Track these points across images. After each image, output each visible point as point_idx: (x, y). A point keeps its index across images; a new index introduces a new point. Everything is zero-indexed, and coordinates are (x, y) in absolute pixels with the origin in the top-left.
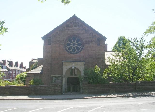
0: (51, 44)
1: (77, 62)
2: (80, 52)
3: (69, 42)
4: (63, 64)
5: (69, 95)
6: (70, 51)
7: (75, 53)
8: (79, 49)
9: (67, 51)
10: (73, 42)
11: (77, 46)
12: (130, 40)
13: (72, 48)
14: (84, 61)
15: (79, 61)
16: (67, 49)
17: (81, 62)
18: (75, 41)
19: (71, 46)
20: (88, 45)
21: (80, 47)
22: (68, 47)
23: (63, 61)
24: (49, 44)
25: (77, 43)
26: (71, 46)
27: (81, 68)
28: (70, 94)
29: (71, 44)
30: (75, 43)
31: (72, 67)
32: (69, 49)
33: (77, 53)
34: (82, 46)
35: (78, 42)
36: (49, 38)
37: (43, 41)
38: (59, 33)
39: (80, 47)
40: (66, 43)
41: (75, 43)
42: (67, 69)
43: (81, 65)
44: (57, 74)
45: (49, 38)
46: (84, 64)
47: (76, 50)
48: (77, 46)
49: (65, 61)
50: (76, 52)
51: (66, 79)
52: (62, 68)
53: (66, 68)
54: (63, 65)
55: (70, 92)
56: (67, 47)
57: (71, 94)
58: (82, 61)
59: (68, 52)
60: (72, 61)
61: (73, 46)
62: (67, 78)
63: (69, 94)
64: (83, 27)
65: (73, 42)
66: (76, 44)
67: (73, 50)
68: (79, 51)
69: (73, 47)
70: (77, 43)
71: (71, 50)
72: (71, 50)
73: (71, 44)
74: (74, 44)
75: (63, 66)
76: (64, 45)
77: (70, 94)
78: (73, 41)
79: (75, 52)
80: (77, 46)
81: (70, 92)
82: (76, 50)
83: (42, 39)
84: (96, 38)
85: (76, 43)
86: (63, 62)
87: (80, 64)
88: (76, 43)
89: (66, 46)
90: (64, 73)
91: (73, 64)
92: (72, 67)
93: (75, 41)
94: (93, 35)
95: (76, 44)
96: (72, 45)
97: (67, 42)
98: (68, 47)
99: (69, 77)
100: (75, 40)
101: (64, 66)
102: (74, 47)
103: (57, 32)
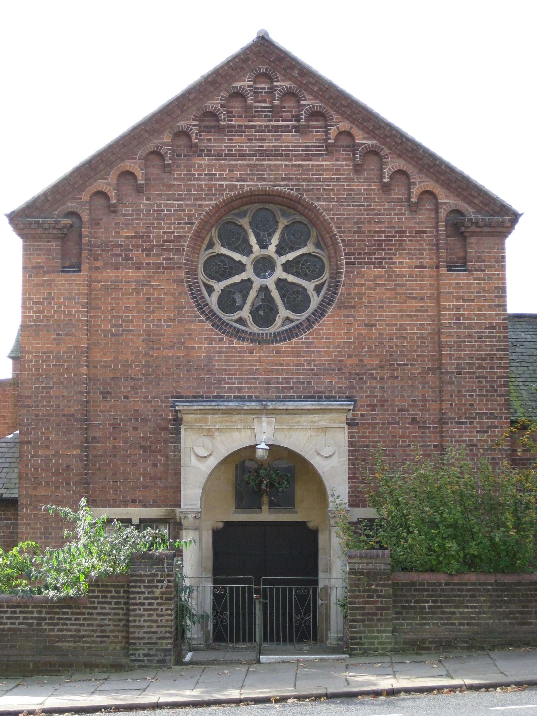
0: (85, 267)
1: (291, 406)
2: (309, 327)
3: (224, 251)
4: (178, 422)
5: (243, 669)
6: (236, 316)
7: (279, 337)
8: (307, 300)
9: (211, 316)
10: (256, 247)
11: (291, 278)
12: (343, 417)
13: (252, 294)
14: (349, 398)
15: (310, 398)
16: (213, 301)
17: (324, 405)
18: (275, 240)
19: (237, 279)
20: (370, 272)
21: (309, 286)
22: (219, 286)
23: (179, 398)
24: (65, 270)
25: (291, 256)
26: (237, 279)
27: (327, 452)
28: (252, 655)
29: (240, 267)
30: (275, 256)
31: (253, 448)
32: (228, 302)
33: (290, 334)
34: (326, 276)
35: (292, 249)
36: (69, 222)
37: (17, 243)
38: (141, 180)
39: (309, 286)
40: (204, 255)
41: (275, 256)
42: (213, 462)
43: (323, 423)
44: (135, 502)
45: (69, 222)
46: (351, 423)
47: (283, 312)
48: (284, 275)
49: (197, 398)
50: (279, 321)
51: (208, 538)
52: (178, 451)
53: (202, 452)
54: (178, 433)
55: (251, 639)
56: (210, 289)
57: (258, 662)
58: (330, 398)
59: (220, 325)
60: (250, 399)
61: (257, 282)
62: (217, 534)
63: (239, 663)
64: (333, 132)
65: (256, 247)
66: (283, 259)
67: (254, 313)
68: (201, 266)
69: (256, 286)
70: (291, 256)
71: (241, 308)
72: (245, 313)
73: (240, 267)
74: (264, 266)
75: (178, 441)
76: (182, 273)
77: (250, 662)
78: (253, 240)
79: (277, 326)
80: (291, 278)
81: (251, 639)
82: (283, 312)
83: (10, 228)
84: (437, 211)
85: (280, 251)
86: (180, 406)
87: (316, 417)
88: (280, 251)
89: (202, 276)
90: (191, 494)
91: (264, 419)
92: (253, 448)
93: (275, 240)
94: (409, 193)
95: (283, 259)
96: (249, 273)
97: (211, 245)
98: (219, 286)
99: (228, 524)
100: (270, 235)
101: (189, 439)
102: (264, 289)
103: (130, 174)
